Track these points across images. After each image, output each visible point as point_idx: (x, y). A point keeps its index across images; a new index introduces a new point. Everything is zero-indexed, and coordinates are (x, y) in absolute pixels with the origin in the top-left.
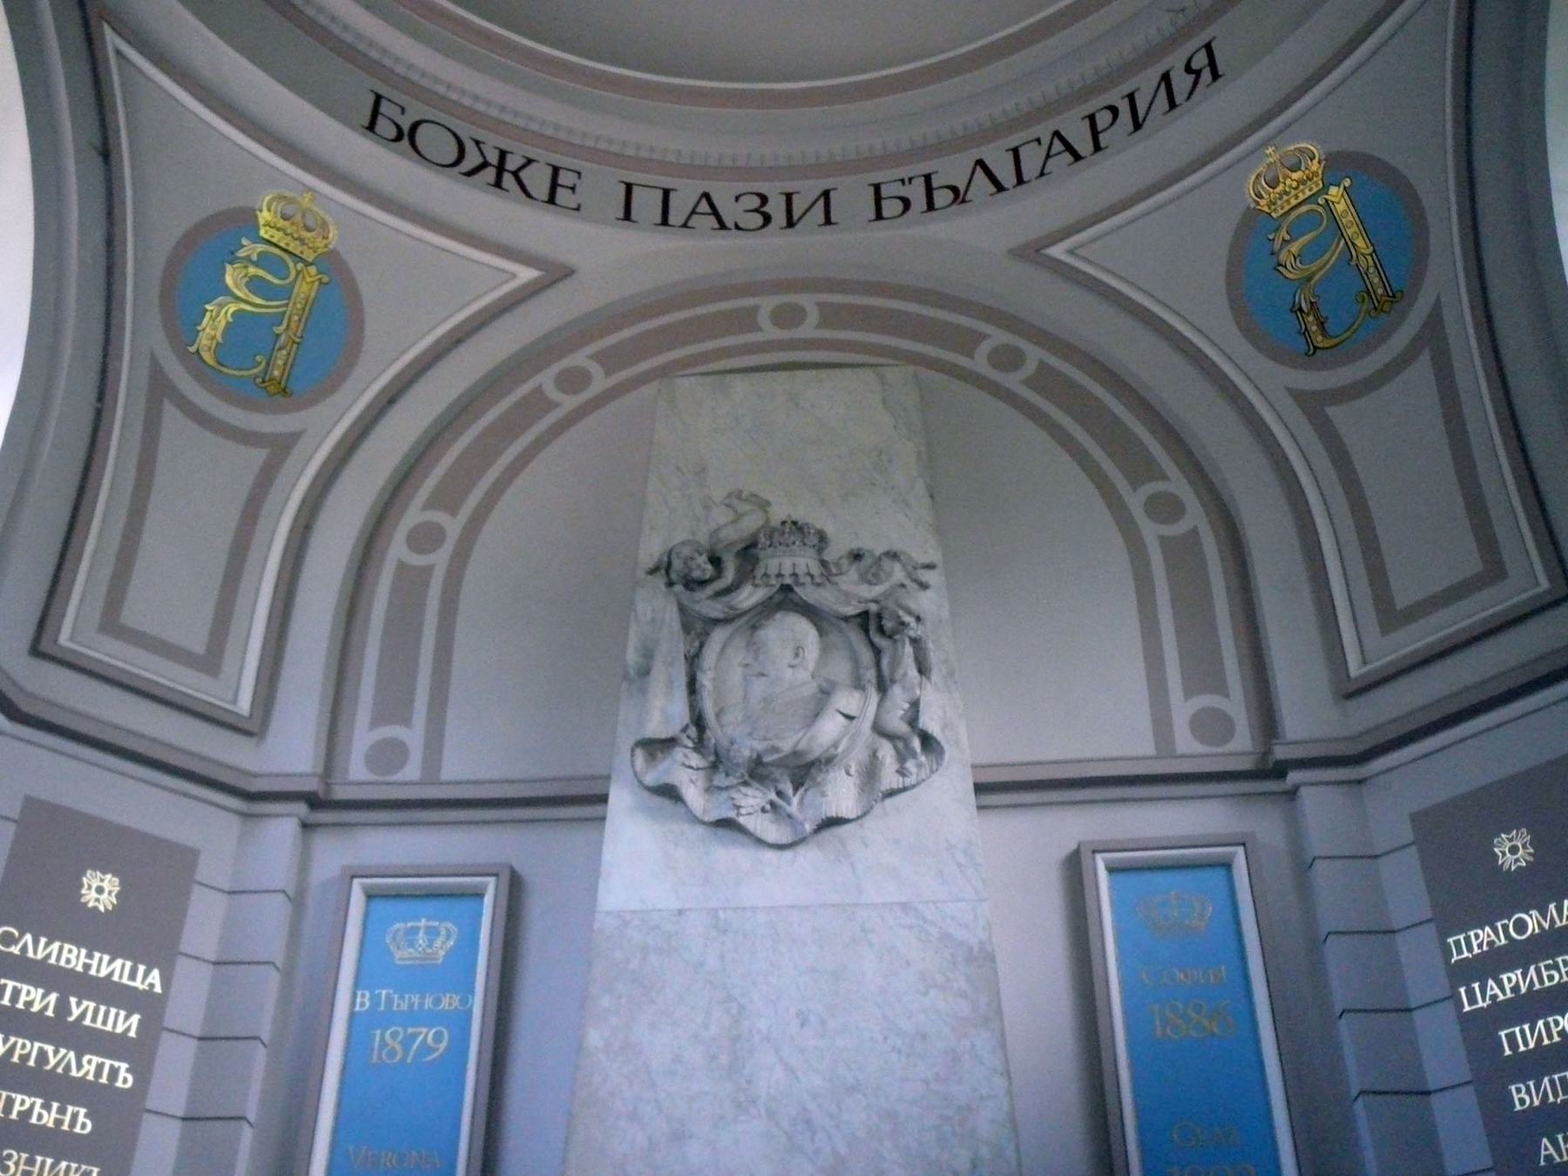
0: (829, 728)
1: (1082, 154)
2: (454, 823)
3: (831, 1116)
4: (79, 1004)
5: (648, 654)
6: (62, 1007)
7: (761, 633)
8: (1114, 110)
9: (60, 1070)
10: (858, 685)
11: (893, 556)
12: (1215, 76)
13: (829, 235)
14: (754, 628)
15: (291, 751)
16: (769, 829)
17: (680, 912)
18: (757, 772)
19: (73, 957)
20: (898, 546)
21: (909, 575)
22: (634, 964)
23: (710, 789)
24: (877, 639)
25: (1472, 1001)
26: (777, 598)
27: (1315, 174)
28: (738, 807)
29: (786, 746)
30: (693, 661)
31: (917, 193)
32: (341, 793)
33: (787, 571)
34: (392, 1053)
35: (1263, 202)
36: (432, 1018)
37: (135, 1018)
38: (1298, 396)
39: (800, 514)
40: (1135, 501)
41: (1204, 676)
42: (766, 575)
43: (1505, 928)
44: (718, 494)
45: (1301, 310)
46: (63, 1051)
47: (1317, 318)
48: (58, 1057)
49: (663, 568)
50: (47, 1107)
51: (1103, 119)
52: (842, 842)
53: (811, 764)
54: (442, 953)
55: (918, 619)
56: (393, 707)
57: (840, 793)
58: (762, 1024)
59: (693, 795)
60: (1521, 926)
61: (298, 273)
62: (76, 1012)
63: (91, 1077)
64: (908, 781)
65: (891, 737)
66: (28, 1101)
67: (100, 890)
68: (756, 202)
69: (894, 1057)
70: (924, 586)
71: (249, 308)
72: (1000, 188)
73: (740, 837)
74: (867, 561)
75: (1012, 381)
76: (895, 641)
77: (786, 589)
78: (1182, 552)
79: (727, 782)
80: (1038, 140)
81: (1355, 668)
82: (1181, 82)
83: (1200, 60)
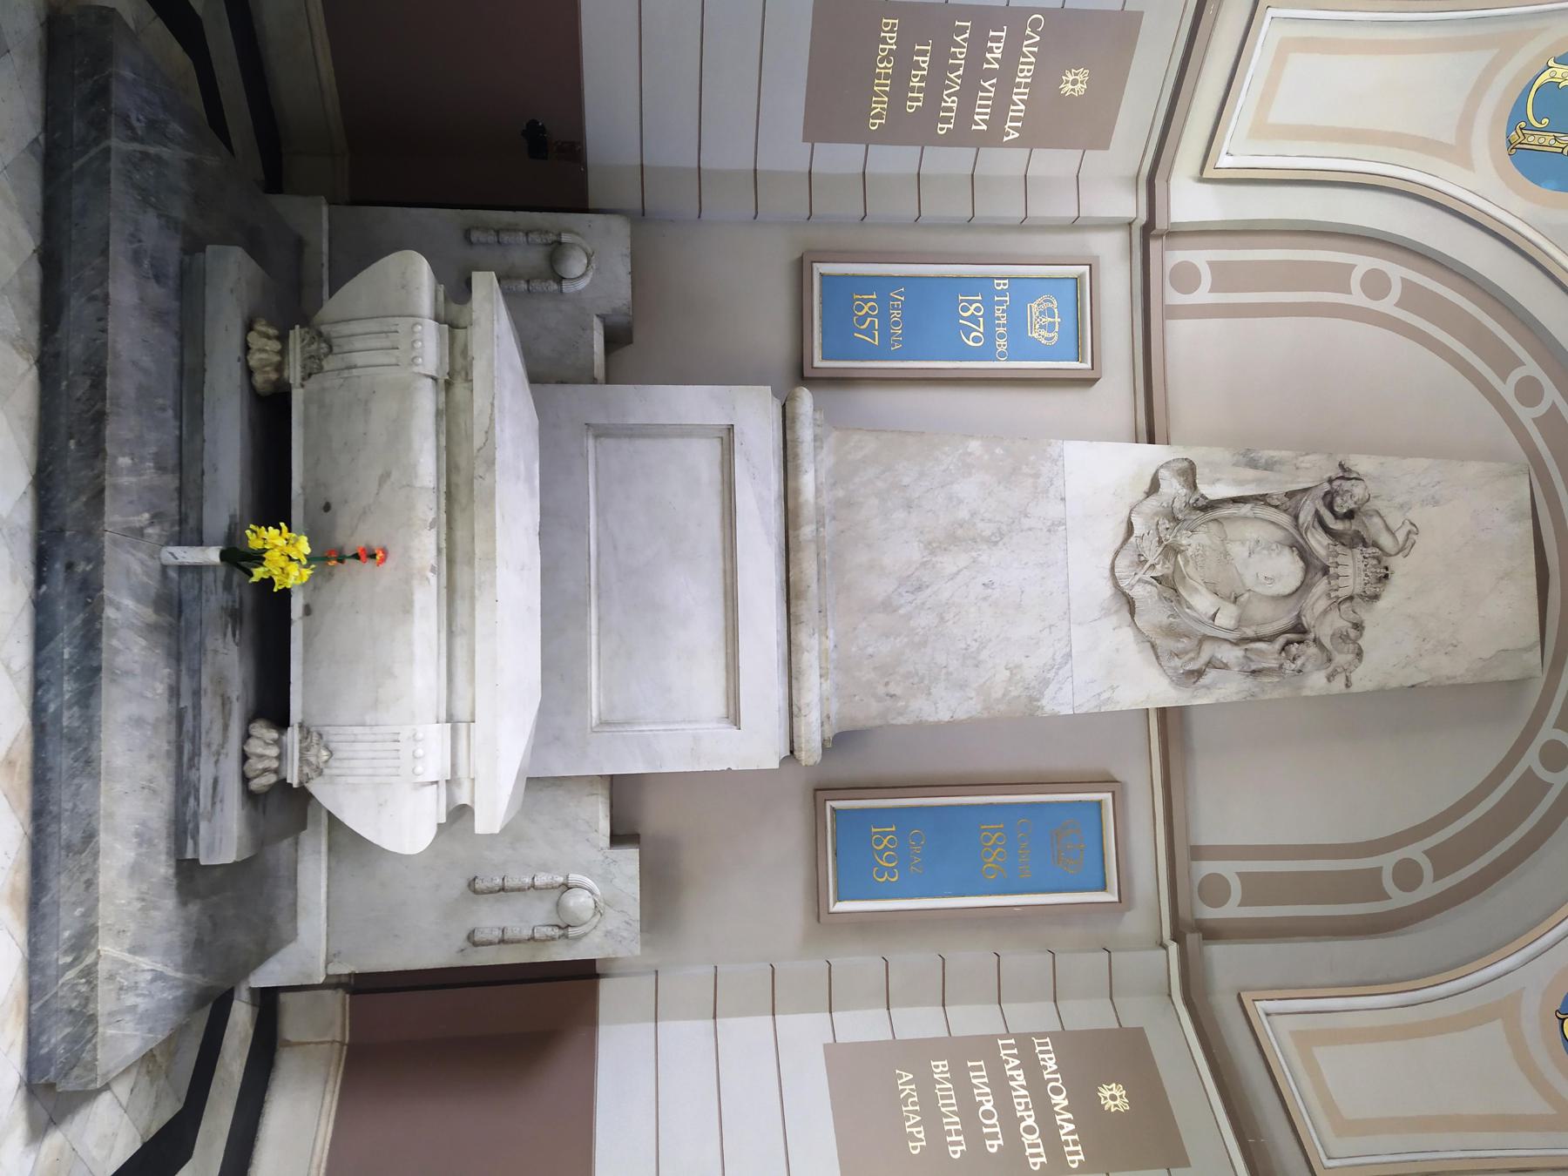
0: (1203, 602)
5: (1269, 466)
6: (990, 74)
7: (1287, 551)
10: (1241, 621)
11: (1359, 654)
15: (1188, 201)
17: (1063, 499)
22: (1025, 469)
25: (1006, 1047)
29: (1190, 570)
30: (1261, 499)
32: (1155, 246)
33: (1340, 570)
34: (965, 309)
36: (990, 334)
39: (1396, 579)
40: (1415, 852)
41: (1256, 888)
43: (1056, 1080)
49: (1346, 473)
50: (923, 78)
52: (1116, 612)
54: (1035, 335)
56: (1225, 276)
58: (984, 558)
59: (1153, 503)
60: (1057, 1091)
67: (1075, 83)
70: (1330, 678)
74: (1353, 633)
78: (1369, 885)
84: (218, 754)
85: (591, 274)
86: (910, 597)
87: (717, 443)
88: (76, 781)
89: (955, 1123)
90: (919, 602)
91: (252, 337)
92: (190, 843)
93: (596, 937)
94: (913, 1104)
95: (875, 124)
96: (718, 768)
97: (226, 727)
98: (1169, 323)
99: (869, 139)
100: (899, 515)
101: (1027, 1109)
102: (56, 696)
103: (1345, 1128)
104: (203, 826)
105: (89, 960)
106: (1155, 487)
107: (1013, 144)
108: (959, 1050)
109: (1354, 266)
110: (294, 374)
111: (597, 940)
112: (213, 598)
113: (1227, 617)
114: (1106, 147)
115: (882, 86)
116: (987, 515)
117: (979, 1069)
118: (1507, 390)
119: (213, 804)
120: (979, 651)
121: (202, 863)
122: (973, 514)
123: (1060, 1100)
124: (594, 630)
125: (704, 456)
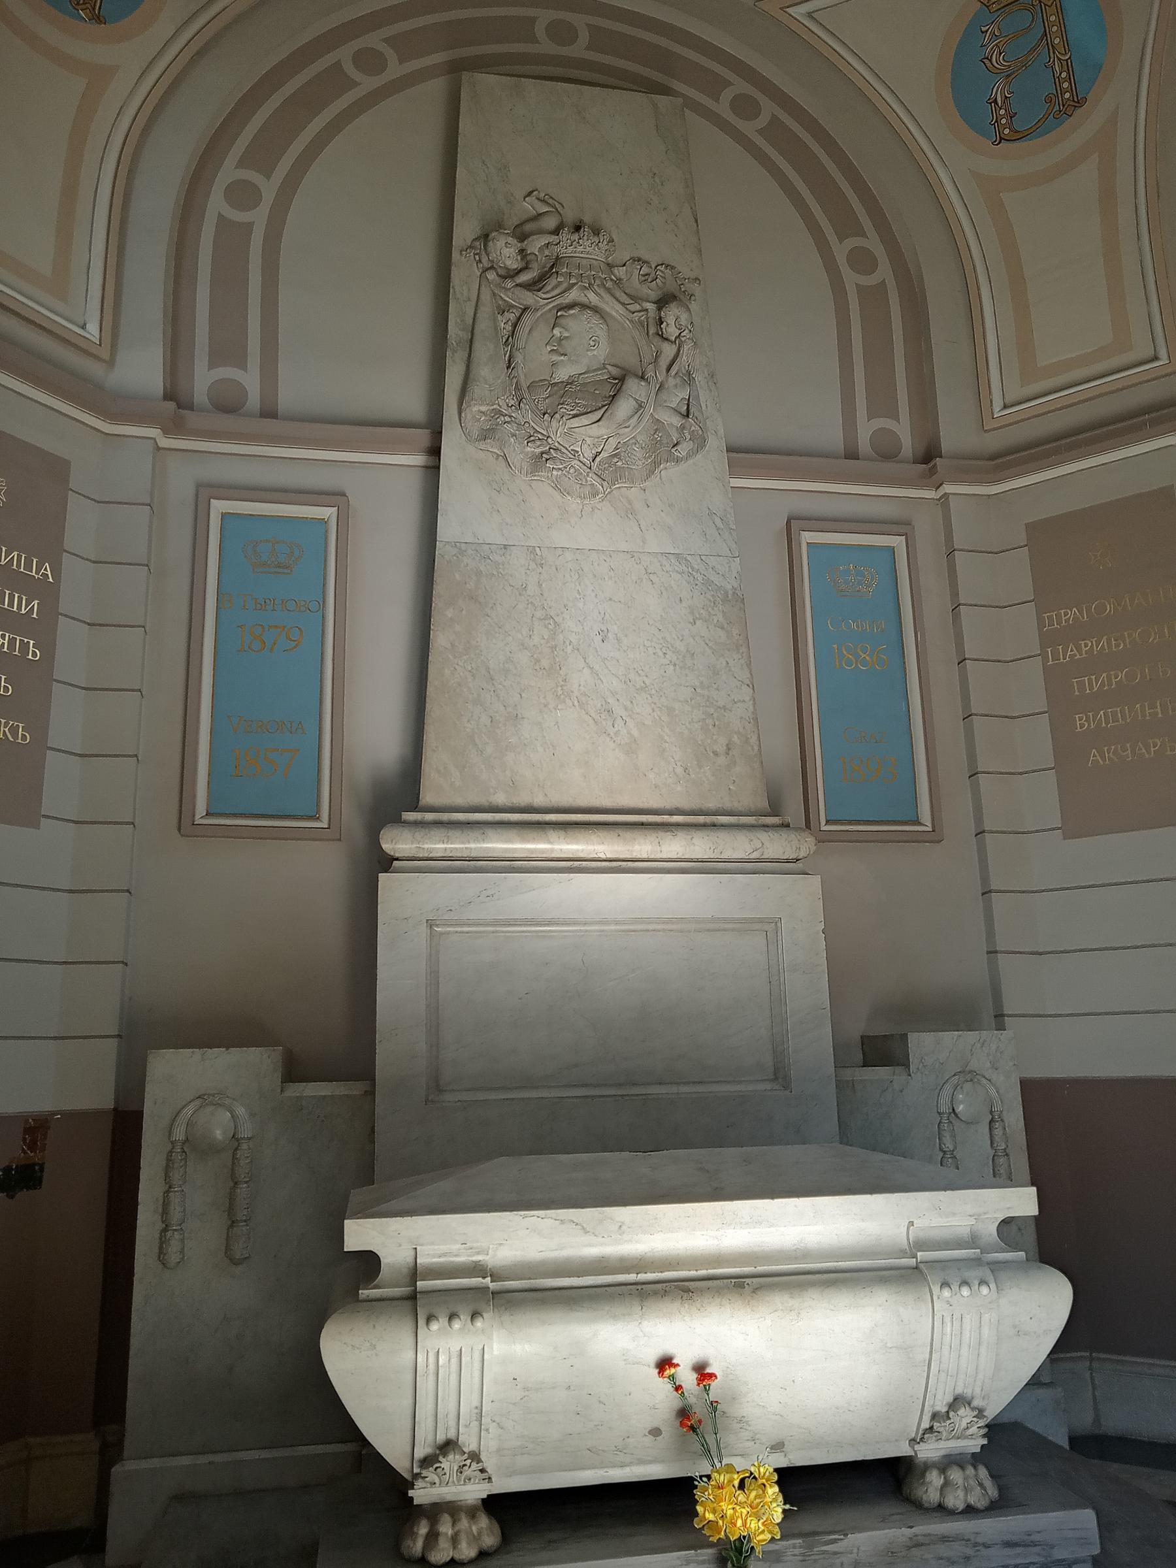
3: (626, 709)
17: (505, 547)
40: (841, 251)
45: (995, 101)
58: (573, 638)
75: (749, 128)
78: (873, 297)
84: (976, 1544)
86: (619, 722)
89: (1143, 707)
90: (624, 714)
95: (24, 736)
107: (56, 572)
109: (587, 48)
110: (475, 1492)
114: (67, 463)
116: (525, 631)
118: (368, 83)
119: (1034, 1544)
124: (674, 1089)
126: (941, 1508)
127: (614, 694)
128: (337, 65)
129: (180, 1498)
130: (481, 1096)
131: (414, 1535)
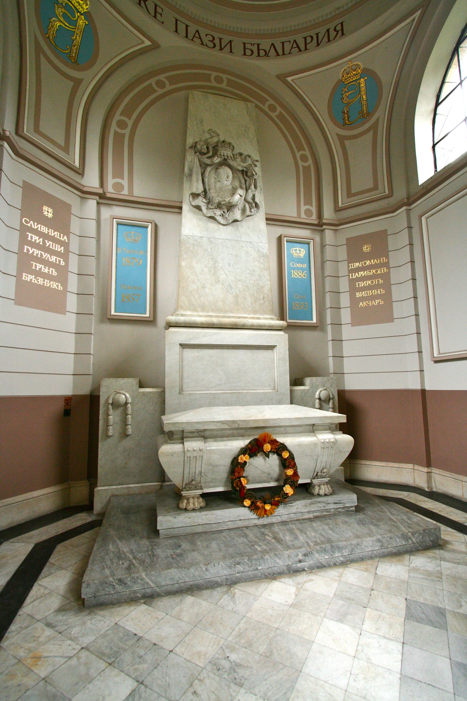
1: (302, 50)
2: (133, 207)
4: (48, 242)
5: (191, 171)
6: (44, 243)
7: (219, 170)
8: (312, 37)
9: (46, 259)
10: (241, 187)
12: (343, 34)
13: (230, 56)
14: (217, 169)
16: (222, 221)
17: (201, 237)
18: (219, 206)
19: (44, 229)
20: (250, 154)
21: (253, 162)
23: (208, 208)
24: (246, 177)
25: (352, 276)
26: (223, 162)
27: (359, 73)
28: (215, 214)
29: (227, 200)
30: (203, 174)
31: (255, 49)
33: (225, 155)
35: (343, 78)
37: (62, 248)
38: (338, 135)
40: (298, 155)
42: (220, 155)
43: (362, 263)
44: (206, 130)
46: (46, 254)
47: (347, 115)
48: (46, 256)
49: (194, 146)
50: (45, 268)
51: (309, 40)
52: (237, 226)
53: (232, 206)
55: (256, 174)
57: (237, 214)
58: (220, 265)
59: (204, 208)
60: (365, 263)
61: (78, 17)
62: (48, 244)
63: (54, 261)
64: (252, 214)
65: (249, 203)
66: (41, 266)
68: (211, 39)
69: (248, 275)
70: (256, 166)
71: (64, 26)
72: (278, 55)
73: (214, 221)
74: (243, 156)
76: (250, 179)
77: (225, 160)
78: (307, 170)
79: (212, 207)
80: (290, 41)
81: (340, 205)
82: (332, 34)
83: (339, 28)
85: (124, 392)
86: (233, 289)
87: (185, 350)
88: (363, 547)
89: (375, 291)
91: (189, 508)
92: (351, 509)
93: (332, 390)
94: (369, 302)
95: (61, 288)
96: (288, 353)
97: (319, 502)
98: (135, 194)
99: (65, 291)
100: (207, 290)
101: (371, 272)
102: (338, 558)
103: (375, 188)
104: (347, 505)
105: (410, 534)
106: (198, 208)
107: (68, 239)
108: (353, 290)
111: (333, 389)
112: (281, 511)
113: (241, 192)
115: (47, 283)
116: (207, 262)
117: (359, 284)
118: (160, 91)
120: (250, 270)
121: (356, 504)
122: (206, 267)
123: (368, 263)
125: (189, 354)
126: (319, 495)
127: (232, 281)
128: (151, 84)
129: (113, 496)
130: (194, 392)
131: (183, 502)
